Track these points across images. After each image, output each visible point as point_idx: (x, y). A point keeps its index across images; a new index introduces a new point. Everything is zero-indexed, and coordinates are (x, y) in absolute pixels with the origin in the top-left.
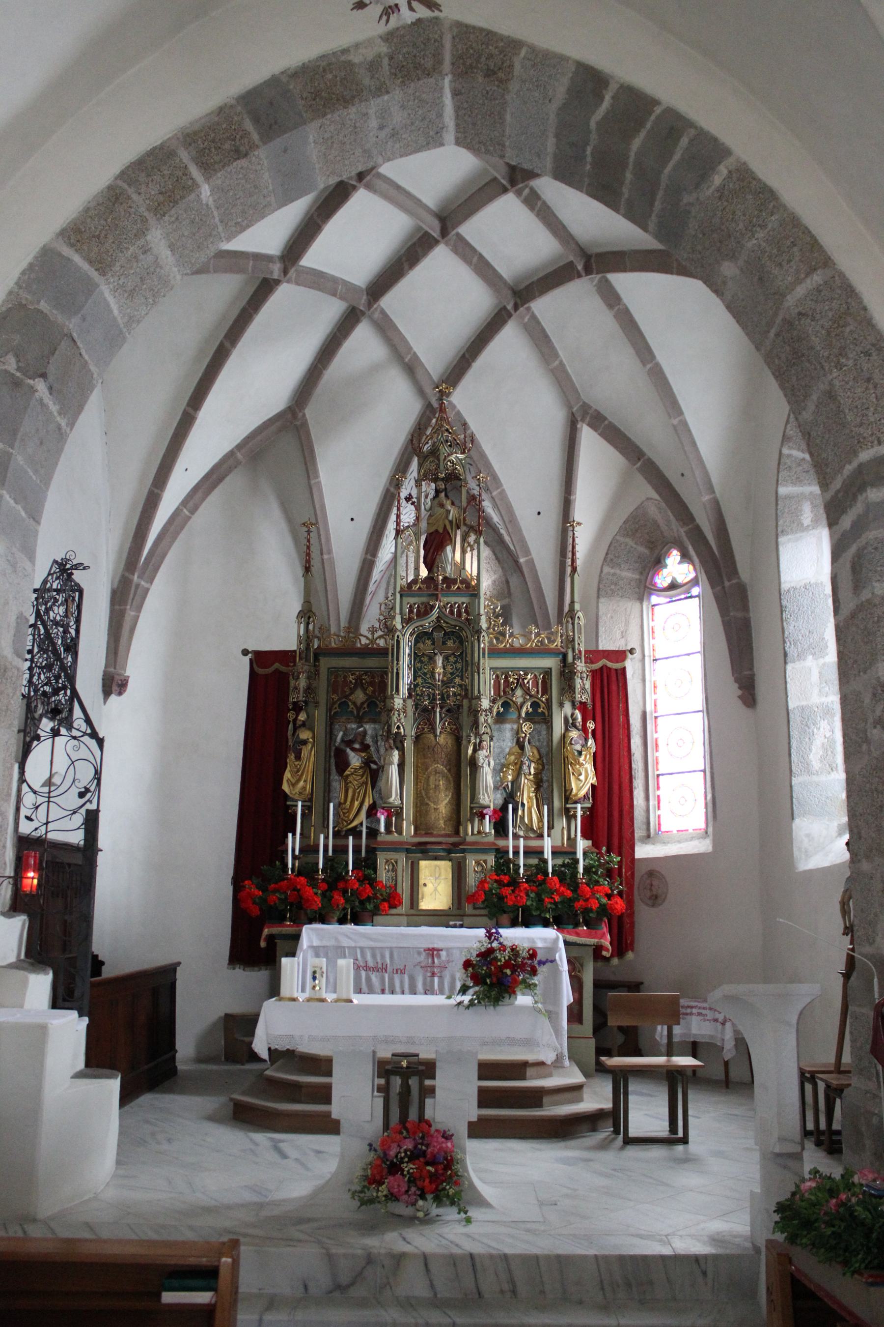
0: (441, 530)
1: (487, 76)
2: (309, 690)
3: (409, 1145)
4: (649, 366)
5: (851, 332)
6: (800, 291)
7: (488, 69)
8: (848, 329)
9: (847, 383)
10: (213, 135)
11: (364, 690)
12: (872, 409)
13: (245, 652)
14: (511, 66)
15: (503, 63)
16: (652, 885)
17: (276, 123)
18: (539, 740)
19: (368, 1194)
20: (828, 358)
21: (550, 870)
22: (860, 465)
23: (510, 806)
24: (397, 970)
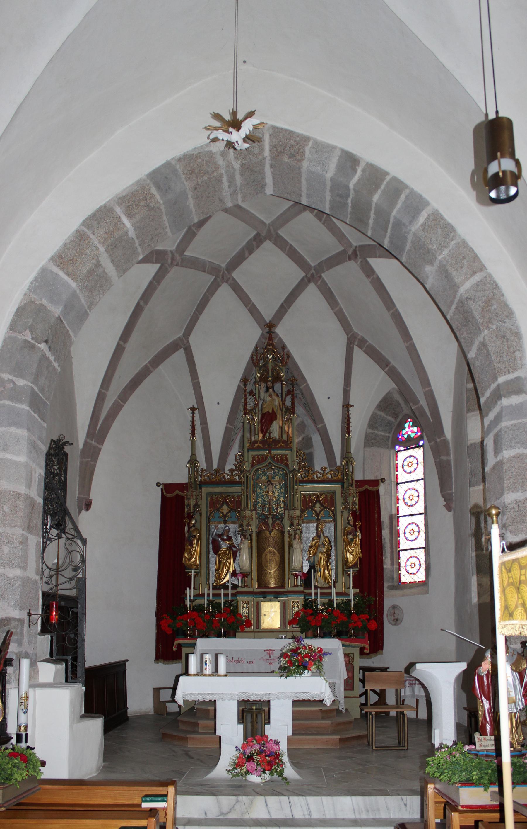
0: (271, 411)
1: (290, 157)
2: (197, 505)
3: (257, 747)
4: (391, 312)
5: (495, 309)
6: (468, 285)
7: (291, 154)
8: (493, 308)
9: (492, 338)
10: (134, 198)
11: (228, 505)
12: (505, 353)
13: (158, 484)
14: (304, 152)
15: (299, 150)
16: (394, 613)
17: (169, 188)
18: (329, 532)
19: (236, 771)
20: (482, 323)
21: (335, 606)
22: (498, 385)
23: (313, 570)
24: (250, 662)
